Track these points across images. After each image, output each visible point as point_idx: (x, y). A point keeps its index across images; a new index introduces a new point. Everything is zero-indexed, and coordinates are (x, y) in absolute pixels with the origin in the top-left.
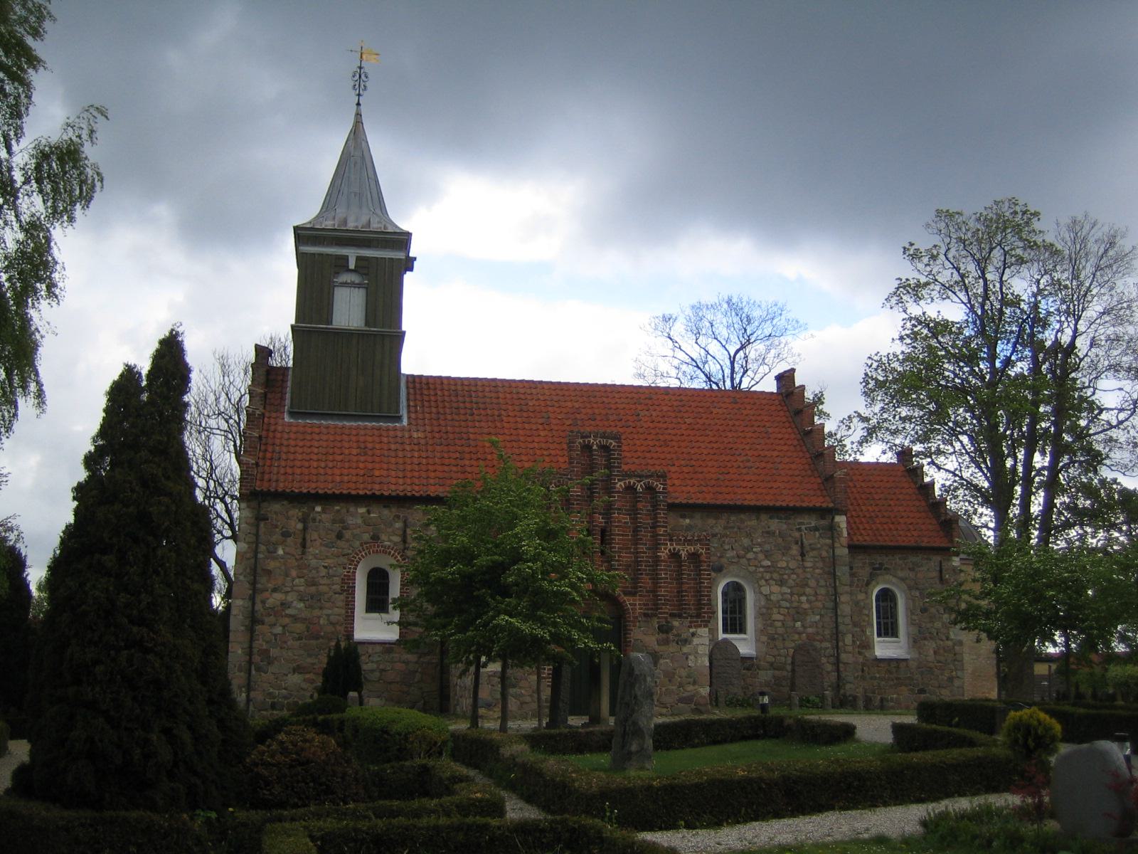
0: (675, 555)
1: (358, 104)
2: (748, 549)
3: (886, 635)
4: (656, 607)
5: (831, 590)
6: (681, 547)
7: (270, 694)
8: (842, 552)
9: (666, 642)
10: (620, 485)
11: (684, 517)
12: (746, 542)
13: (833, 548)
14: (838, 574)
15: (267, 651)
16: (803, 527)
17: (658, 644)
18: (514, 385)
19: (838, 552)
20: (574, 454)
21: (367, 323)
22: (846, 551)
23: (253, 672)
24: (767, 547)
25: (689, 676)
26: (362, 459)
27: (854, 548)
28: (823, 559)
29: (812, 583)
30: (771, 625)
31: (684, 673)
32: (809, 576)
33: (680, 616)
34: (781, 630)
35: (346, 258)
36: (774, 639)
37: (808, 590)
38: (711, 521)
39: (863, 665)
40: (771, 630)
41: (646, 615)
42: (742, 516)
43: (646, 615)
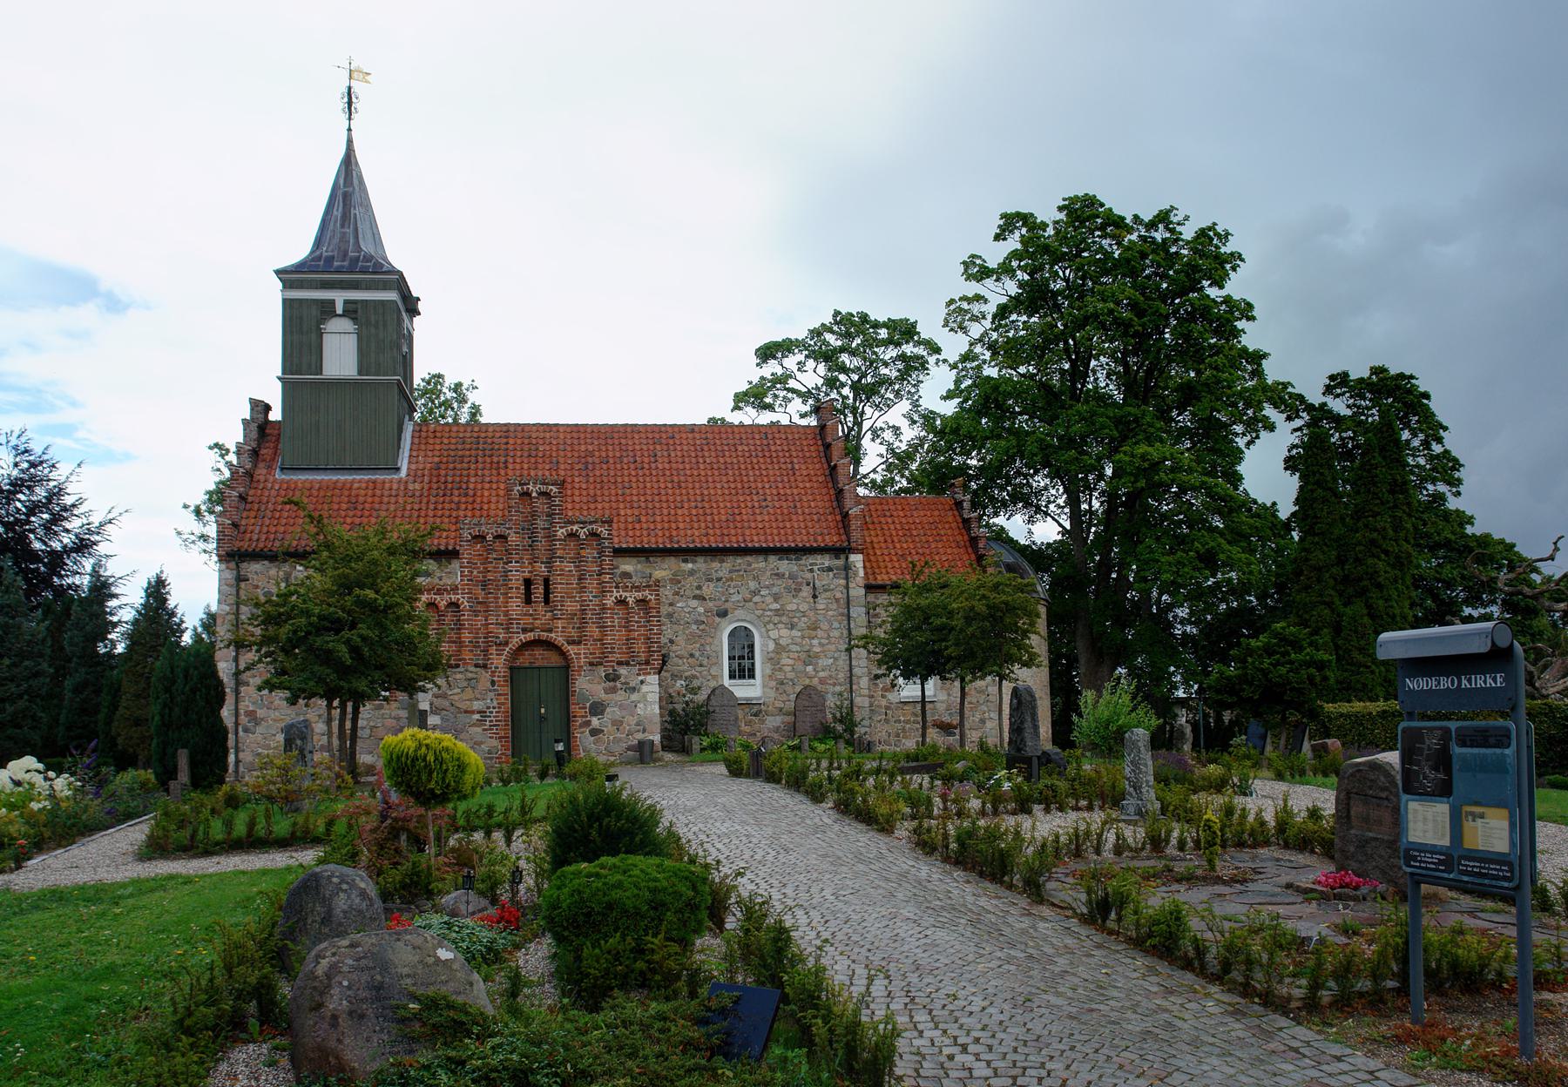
0: (621, 602)
1: (349, 130)
2: (755, 593)
3: (742, 677)
4: (604, 655)
5: (845, 632)
6: (628, 594)
7: (259, 754)
8: (858, 592)
9: (614, 690)
10: (561, 533)
11: (686, 561)
12: (753, 585)
13: (847, 587)
14: (852, 614)
15: (254, 712)
16: (816, 568)
17: (606, 693)
18: (526, 429)
19: (852, 592)
20: (512, 503)
21: (360, 373)
22: (863, 591)
23: (241, 733)
24: (775, 590)
25: (638, 724)
26: (351, 514)
27: (870, 588)
28: (837, 600)
29: (825, 626)
30: (780, 670)
31: (633, 720)
32: (820, 618)
33: (627, 664)
34: (791, 675)
35: (332, 302)
36: (782, 683)
37: (820, 633)
38: (716, 565)
39: (887, 708)
40: (780, 675)
41: (591, 664)
42: (749, 558)
43: (591, 664)
